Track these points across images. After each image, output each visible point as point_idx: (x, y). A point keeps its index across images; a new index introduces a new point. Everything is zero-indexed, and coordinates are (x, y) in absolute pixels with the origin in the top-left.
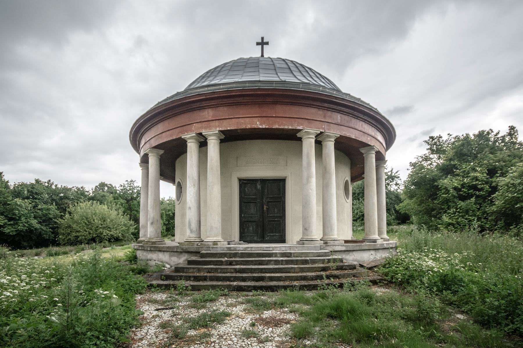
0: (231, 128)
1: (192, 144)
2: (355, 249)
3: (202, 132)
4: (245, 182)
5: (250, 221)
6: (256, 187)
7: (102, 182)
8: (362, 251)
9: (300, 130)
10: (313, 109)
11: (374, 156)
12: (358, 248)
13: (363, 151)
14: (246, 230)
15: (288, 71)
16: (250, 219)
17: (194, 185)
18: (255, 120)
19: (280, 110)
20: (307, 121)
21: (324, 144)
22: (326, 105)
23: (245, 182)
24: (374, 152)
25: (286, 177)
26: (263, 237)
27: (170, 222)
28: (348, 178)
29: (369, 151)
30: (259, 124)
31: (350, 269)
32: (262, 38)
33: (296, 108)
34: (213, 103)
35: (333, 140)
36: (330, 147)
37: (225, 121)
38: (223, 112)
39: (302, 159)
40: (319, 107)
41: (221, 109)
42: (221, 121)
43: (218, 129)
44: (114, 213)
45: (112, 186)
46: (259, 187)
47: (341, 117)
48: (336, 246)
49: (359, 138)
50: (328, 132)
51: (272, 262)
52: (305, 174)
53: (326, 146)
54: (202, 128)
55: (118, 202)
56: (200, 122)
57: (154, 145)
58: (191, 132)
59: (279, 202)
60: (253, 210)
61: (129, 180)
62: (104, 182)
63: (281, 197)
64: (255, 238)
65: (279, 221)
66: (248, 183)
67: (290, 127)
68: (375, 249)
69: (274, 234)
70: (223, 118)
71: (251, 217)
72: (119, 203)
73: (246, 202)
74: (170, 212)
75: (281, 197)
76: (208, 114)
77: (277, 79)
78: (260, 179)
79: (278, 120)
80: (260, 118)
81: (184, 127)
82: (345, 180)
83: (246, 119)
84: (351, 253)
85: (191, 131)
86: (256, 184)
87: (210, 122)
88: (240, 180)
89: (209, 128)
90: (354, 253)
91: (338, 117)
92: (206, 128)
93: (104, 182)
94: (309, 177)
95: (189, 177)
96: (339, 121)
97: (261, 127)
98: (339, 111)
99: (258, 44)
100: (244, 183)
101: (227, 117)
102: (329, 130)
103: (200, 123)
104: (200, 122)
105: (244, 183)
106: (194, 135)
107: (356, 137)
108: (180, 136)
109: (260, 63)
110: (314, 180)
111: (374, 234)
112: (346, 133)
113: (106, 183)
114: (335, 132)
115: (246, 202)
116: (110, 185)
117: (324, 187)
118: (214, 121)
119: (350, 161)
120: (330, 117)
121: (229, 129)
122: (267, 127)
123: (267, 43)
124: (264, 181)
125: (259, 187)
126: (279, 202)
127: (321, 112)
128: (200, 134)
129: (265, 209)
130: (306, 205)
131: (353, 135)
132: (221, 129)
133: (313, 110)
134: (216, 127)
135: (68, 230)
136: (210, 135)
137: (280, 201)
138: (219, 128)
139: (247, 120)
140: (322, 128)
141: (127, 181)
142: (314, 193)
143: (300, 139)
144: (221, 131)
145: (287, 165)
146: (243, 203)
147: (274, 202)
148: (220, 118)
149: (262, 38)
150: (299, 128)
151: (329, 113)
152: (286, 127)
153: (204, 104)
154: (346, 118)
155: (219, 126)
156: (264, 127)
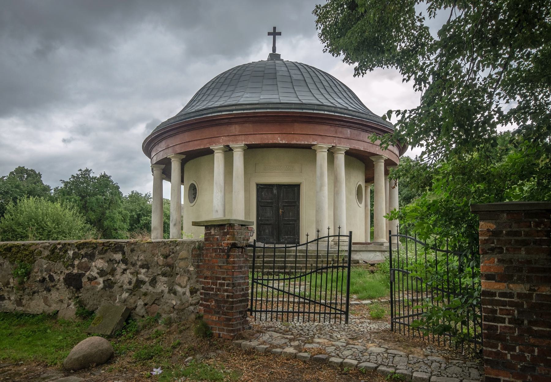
0: (256, 143)
1: (220, 154)
2: (361, 249)
3: (228, 144)
4: (262, 186)
5: (267, 224)
6: (272, 193)
7: (19, 167)
8: (368, 252)
9: (314, 145)
10: (325, 126)
11: (383, 164)
12: (364, 249)
13: (373, 158)
14: (262, 232)
15: (303, 83)
16: (267, 223)
17: (221, 191)
18: (277, 136)
19: (298, 128)
20: (320, 137)
21: (336, 155)
22: (337, 123)
23: (262, 186)
24: (383, 161)
25: (301, 183)
26: (279, 240)
27: (134, 227)
28: (362, 183)
29: (379, 159)
30: (280, 140)
31: (354, 263)
32: (275, 28)
33: (311, 126)
34: (239, 120)
35: (343, 152)
36: (341, 158)
37: (250, 136)
38: (249, 128)
39: (316, 164)
40: (330, 125)
41: (247, 125)
42: (247, 136)
43: (244, 143)
44: (69, 214)
45: (35, 172)
46: (275, 191)
47: (351, 132)
48: (344, 246)
49: (367, 149)
50: (339, 146)
51: (292, 257)
52: (318, 173)
53: (337, 158)
54: (229, 141)
55: (71, 198)
56: (228, 136)
57: (179, 152)
58: (219, 144)
59: (293, 206)
60: (269, 213)
61: (83, 169)
62: (24, 167)
63: (295, 202)
64: (271, 240)
65: (294, 224)
66: (265, 188)
67: (306, 143)
68: (382, 251)
69: (289, 236)
70: (248, 133)
71: (268, 220)
72: (73, 200)
73: (263, 206)
74: (134, 213)
75: (295, 202)
76: (235, 129)
77: (295, 101)
78: (276, 185)
79: (296, 136)
80: (280, 135)
81: (214, 139)
82: (358, 184)
83: (268, 135)
84: (358, 253)
85: (219, 143)
86: (272, 189)
87: (237, 136)
88: (257, 185)
89: (236, 141)
90: (361, 253)
91: (348, 132)
92: (233, 141)
93: (24, 167)
94: (322, 186)
95: (216, 183)
96: (349, 136)
97: (281, 142)
98: (349, 127)
99: (269, 34)
100: (262, 188)
101: (252, 133)
102: (339, 144)
103: (227, 137)
104: (228, 136)
105: (262, 188)
106: (222, 147)
107: (365, 149)
108: (208, 147)
109: (277, 74)
110: (326, 189)
111: (382, 237)
112: (355, 146)
113: (26, 168)
114: (345, 146)
115: (263, 206)
116: (32, 170)
117: (336, 193)
118: (241, 136)
119: (364, 165)
120: (341, 132)
121: (253, 143)
122: (286, 142)
123: (280, 34)
124: (280, 186)
125: (275, 191)
126: (293, 206)
127: (332, 129)
128: (228, 146)
129: (280, 213)
130: (319, 210)
131: (361, 146)
132: (246, 143)
133: (326, 127)
134: (242, 141)
135: (7, 235)
136: (237, 148)
137: (295, 206)
138: (245, 142)
139: (270, 136)
140: (335, 143)
141: (81, 170)
142: (327, 200)
143: (315, 151)
144: (246, 145)
145: (301, 172)
146: (260, 207)
147: (289, 206)
148: (245, 133)
149: (275, 28)
150: (313, 143)
151: (340, 129)
152: (303, 143)
153: (233, 121)
154: (356, 132)
155: (244, 140)
156: (284, 142)
